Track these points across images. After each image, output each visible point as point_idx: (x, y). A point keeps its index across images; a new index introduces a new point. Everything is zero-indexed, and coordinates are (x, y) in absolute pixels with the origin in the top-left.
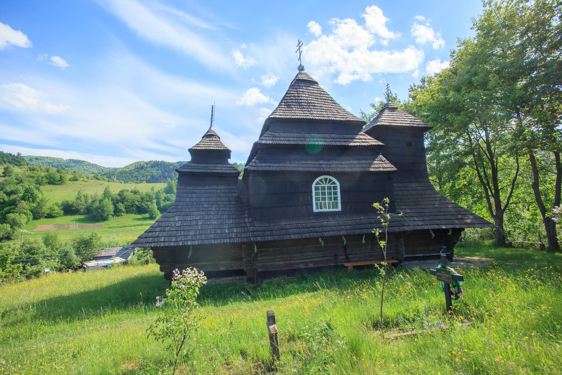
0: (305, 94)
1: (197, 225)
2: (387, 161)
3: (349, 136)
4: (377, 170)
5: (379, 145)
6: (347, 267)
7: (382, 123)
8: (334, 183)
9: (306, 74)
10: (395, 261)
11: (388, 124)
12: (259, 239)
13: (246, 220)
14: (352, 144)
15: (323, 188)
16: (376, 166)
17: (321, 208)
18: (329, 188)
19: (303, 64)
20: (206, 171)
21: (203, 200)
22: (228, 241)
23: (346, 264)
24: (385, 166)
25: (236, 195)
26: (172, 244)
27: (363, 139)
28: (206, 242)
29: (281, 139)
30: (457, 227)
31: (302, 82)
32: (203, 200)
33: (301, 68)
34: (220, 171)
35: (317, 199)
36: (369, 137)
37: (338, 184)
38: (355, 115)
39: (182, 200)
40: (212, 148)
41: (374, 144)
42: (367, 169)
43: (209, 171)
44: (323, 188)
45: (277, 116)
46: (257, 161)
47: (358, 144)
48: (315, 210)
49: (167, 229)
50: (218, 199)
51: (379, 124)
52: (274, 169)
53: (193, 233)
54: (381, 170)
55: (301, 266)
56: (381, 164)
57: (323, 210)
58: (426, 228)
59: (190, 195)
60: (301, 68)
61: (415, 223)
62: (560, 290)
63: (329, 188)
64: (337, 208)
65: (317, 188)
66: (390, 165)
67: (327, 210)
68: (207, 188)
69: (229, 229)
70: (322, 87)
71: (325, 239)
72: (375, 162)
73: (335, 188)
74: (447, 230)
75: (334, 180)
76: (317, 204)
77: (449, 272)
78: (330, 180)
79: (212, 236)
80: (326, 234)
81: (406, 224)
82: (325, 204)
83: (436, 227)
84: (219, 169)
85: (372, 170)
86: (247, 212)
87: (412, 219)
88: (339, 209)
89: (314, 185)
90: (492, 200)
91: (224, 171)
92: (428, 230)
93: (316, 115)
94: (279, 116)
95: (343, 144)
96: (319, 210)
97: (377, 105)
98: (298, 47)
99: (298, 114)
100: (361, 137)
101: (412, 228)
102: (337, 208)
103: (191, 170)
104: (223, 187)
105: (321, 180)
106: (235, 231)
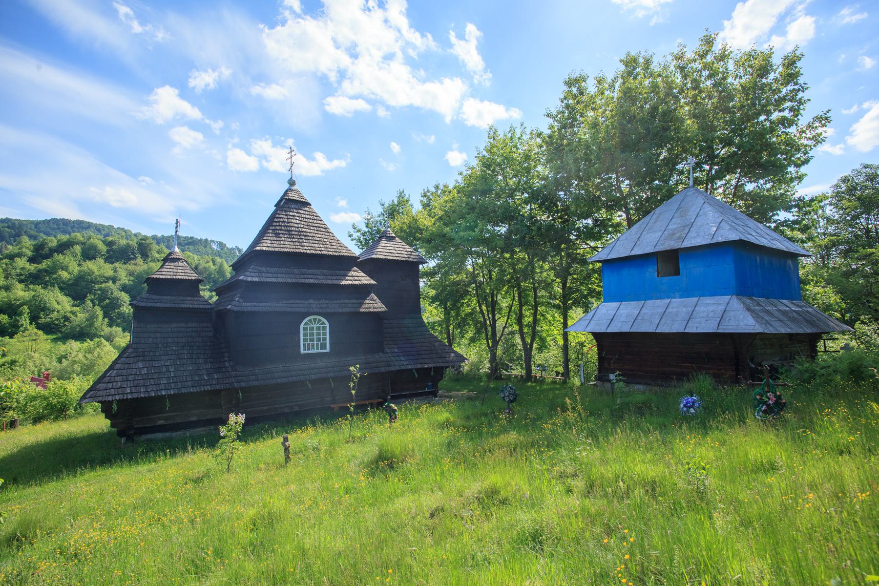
0: (296, 219)
1: (168, 371)
2: (378, 301)
3: (342, 272)
4: (367, 310)
5: (370, 284)
6: (333, 409)
7: (378, 256)
8: (323, 323)
9: (297, 191)
10: (381, 400)
11: (384, 257)
12: (243, 384)
13: (227, 364)
14: (344, 283)
15: (312, 329)
16: (367, 306)
17: (309, 349)
18: (318, 329)
19: (294, 178)
20: (172, 305)
21: (170, 340)
22: (209, 388)
23: (332, 406)
24: (376, 305)
25: (211, 334)
26: (142, 395)
27: (358, 277)
28: (184, 391)
29: (269, 275)
30: (438, 365)
31: (290, 203)
32: (170, 340)
33: (292, 183)
34: (191, 306)
35: (305, 340)
36: (363, 274)
37: (327, 324)
38: (349, 248)
39: (143, 341)
40: (179, 277)
41: (366, 282)
42: (357, 310)
43: (177, 306)
44: (312, 329)
45: (264, 249)
46: (241, 300)
47: (350, 282)
48: (302, 352)
49: (130, 378)
50: (190, 339)
51: (374, 256)
52: (261, 309)
53: (165, 382)
54: (372, 310)
55: (286, 410)
56: (374, 304)
57: (311, 351)
58: (410, 367)
59: (152, 335)
60: (292, 183)
61: (401, 363)
62: (876, 439)
63: (318, 329)
64: (325, 348)
65: (305, 329)
66: (380, 305)
67: (315, 351)
68: (174, 325)
69: (208, 374)
70: (315, 210)
71: (313, 382)
72: (367, 301)
73: (324, 328)
74: (429, 369)
75: (324, 320)
76: (304, 345)
77: (390, 407)
78: (320, 320)
79: (190, 384)
80: (313, 377)
81: (392, 363)
82: (313, 345)
83: (419, 366)
84: (188, 303)
85: (362, 310)
86: (226, 354)
87: (398, 358)
88: (328, 350)
89: (302, 326)
90: (490, 329)
91: (196, 306)
92: (412, 369)
93: (307, 248)
94: (267, 249)
95: (335, 282)
96: (307, 352)
97: (387, 205)
98: (289, 156)
99: (286, 246)
100: (354, 274)
101: (397, 368)
102: (325, 348)
103: (154, 305)
104: (194, 325)
105: (310, 321)
106: (216, 377)
